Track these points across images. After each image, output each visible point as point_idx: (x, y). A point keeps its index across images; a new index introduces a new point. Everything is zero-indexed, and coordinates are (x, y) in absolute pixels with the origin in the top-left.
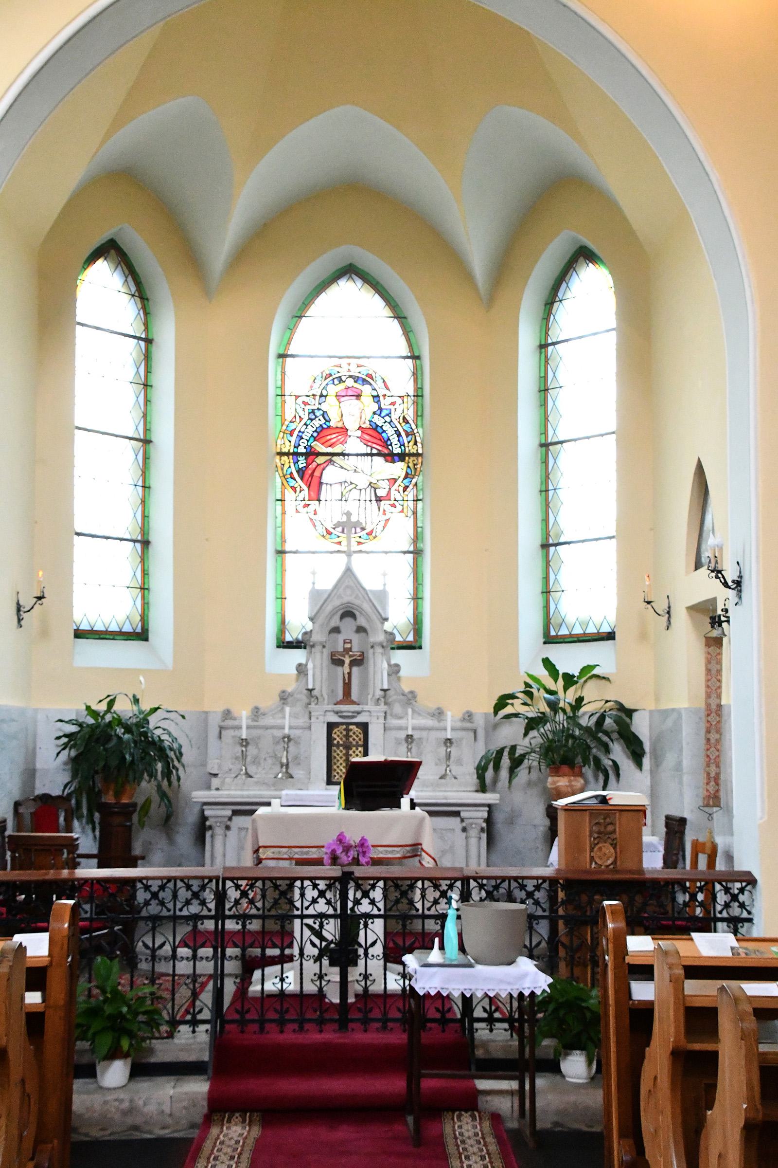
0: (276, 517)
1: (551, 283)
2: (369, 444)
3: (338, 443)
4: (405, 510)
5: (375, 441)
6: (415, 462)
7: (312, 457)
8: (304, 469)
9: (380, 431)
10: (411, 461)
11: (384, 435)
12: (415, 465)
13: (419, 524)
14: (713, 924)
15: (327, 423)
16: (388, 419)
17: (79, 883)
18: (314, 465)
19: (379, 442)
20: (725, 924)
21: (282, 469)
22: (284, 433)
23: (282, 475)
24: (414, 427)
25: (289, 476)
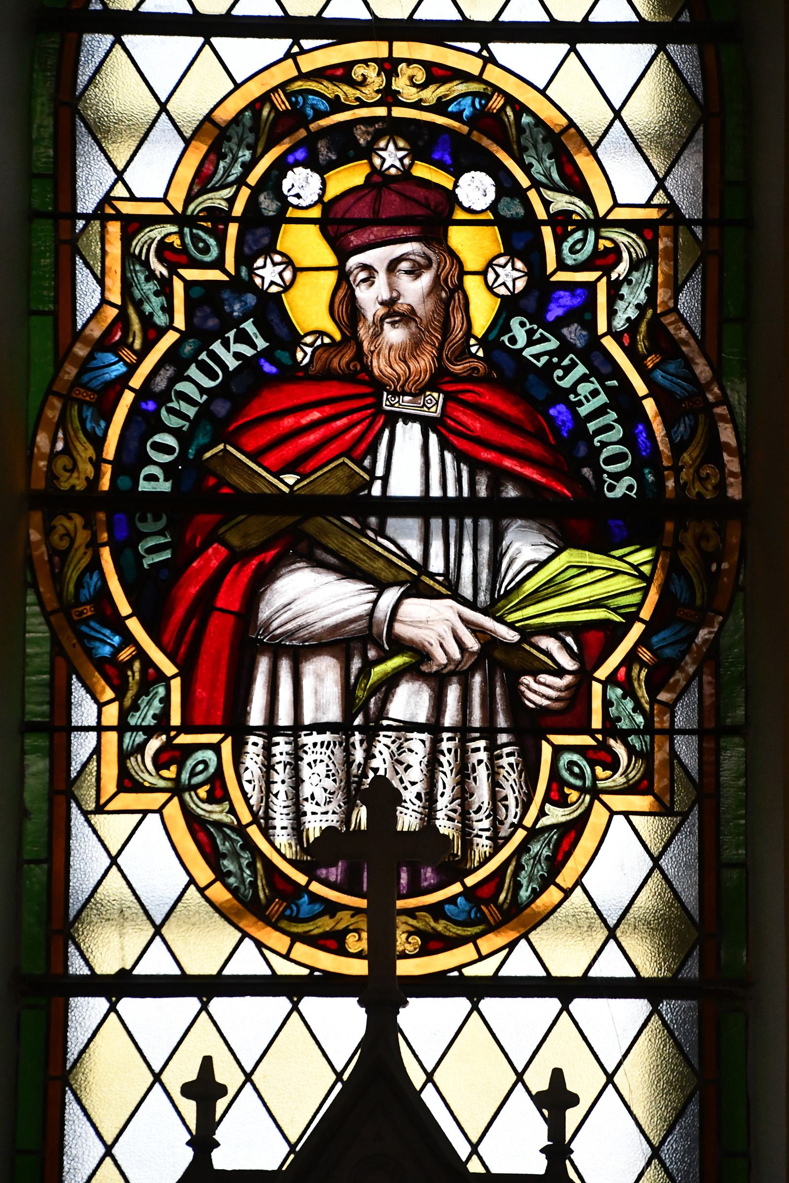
0: (24, 813)
1: (296, 282)
2: (486, 455)
3: (334, 448)
4: (660, 783)
5: (515, 441)
6: (710, 546)
7: (206, 520)
8: (164, 574)
9: (540, 393)
10: (688, 537)
11: (558, 411)
12: (706, 558)
13: (733, 852)
14: (556, 546)
15: (282, 356)
16: (574, 333)
17: (218, 486)
18: (215, 555)
19: (534, 449)
20: (743, 798)
21: (58, 579)
22: (67, 400)
23: (52, 604)
24: (703, 370)
25: (88, 611)
